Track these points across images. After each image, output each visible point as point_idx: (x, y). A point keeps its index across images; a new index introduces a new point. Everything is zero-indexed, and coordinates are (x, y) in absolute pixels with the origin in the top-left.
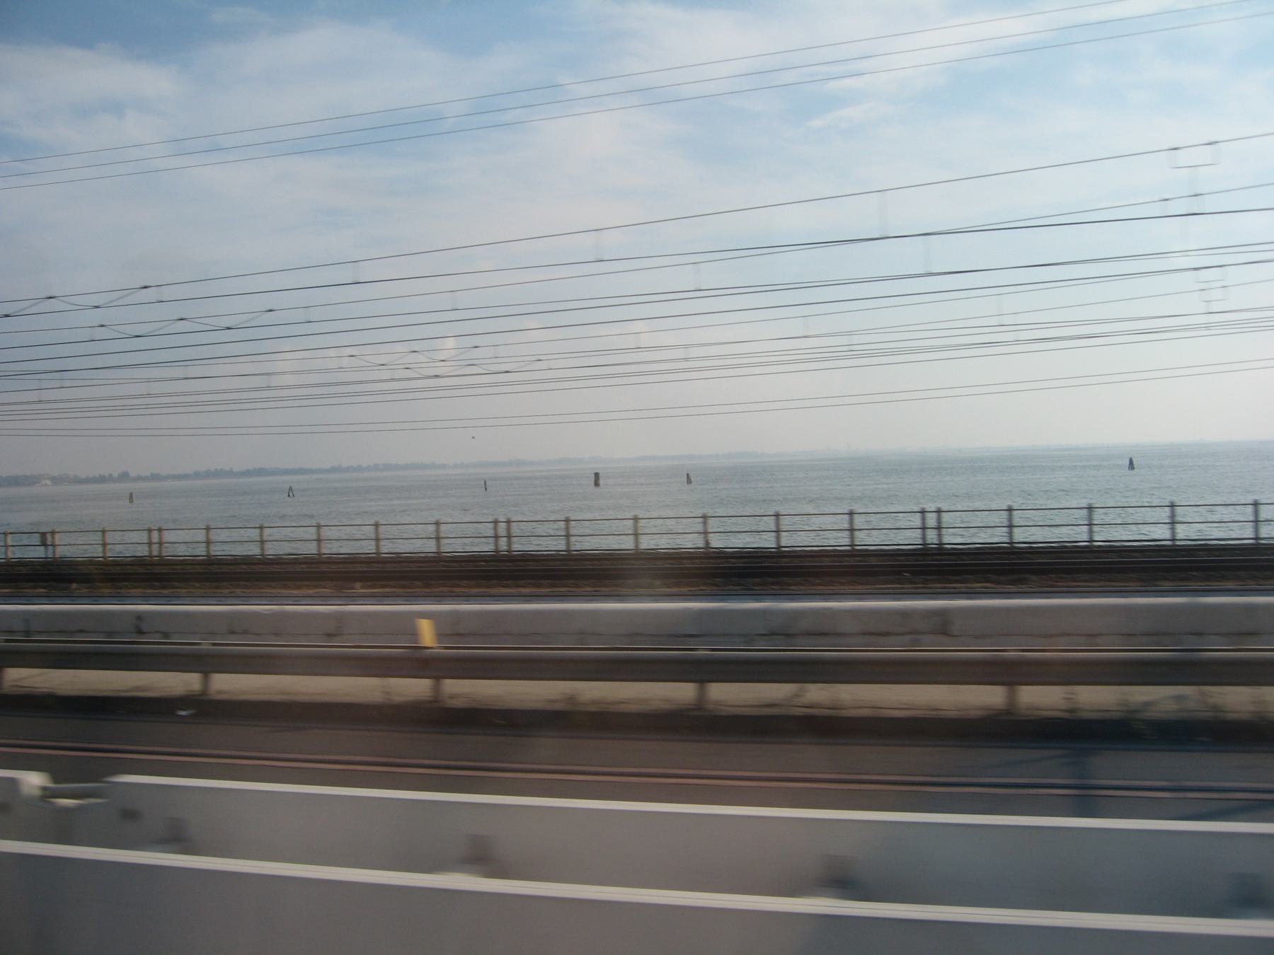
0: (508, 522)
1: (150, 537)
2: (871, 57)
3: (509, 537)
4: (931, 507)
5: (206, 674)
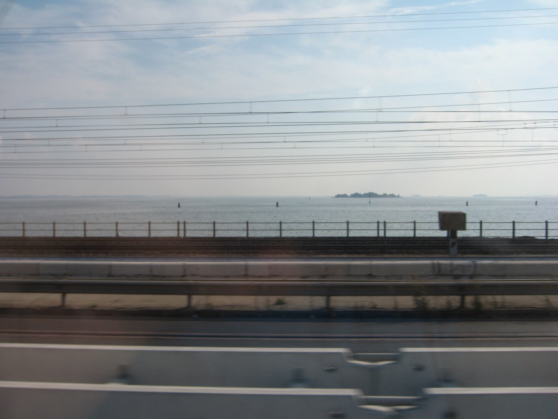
0: (385, 223)
1: (378, 227)
2: (49, 34)
3: (185, 230)
4: (382, 220)
5: (64, 294)
